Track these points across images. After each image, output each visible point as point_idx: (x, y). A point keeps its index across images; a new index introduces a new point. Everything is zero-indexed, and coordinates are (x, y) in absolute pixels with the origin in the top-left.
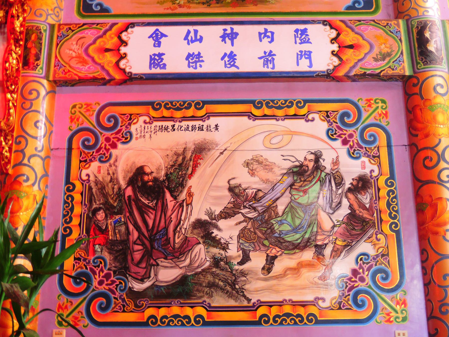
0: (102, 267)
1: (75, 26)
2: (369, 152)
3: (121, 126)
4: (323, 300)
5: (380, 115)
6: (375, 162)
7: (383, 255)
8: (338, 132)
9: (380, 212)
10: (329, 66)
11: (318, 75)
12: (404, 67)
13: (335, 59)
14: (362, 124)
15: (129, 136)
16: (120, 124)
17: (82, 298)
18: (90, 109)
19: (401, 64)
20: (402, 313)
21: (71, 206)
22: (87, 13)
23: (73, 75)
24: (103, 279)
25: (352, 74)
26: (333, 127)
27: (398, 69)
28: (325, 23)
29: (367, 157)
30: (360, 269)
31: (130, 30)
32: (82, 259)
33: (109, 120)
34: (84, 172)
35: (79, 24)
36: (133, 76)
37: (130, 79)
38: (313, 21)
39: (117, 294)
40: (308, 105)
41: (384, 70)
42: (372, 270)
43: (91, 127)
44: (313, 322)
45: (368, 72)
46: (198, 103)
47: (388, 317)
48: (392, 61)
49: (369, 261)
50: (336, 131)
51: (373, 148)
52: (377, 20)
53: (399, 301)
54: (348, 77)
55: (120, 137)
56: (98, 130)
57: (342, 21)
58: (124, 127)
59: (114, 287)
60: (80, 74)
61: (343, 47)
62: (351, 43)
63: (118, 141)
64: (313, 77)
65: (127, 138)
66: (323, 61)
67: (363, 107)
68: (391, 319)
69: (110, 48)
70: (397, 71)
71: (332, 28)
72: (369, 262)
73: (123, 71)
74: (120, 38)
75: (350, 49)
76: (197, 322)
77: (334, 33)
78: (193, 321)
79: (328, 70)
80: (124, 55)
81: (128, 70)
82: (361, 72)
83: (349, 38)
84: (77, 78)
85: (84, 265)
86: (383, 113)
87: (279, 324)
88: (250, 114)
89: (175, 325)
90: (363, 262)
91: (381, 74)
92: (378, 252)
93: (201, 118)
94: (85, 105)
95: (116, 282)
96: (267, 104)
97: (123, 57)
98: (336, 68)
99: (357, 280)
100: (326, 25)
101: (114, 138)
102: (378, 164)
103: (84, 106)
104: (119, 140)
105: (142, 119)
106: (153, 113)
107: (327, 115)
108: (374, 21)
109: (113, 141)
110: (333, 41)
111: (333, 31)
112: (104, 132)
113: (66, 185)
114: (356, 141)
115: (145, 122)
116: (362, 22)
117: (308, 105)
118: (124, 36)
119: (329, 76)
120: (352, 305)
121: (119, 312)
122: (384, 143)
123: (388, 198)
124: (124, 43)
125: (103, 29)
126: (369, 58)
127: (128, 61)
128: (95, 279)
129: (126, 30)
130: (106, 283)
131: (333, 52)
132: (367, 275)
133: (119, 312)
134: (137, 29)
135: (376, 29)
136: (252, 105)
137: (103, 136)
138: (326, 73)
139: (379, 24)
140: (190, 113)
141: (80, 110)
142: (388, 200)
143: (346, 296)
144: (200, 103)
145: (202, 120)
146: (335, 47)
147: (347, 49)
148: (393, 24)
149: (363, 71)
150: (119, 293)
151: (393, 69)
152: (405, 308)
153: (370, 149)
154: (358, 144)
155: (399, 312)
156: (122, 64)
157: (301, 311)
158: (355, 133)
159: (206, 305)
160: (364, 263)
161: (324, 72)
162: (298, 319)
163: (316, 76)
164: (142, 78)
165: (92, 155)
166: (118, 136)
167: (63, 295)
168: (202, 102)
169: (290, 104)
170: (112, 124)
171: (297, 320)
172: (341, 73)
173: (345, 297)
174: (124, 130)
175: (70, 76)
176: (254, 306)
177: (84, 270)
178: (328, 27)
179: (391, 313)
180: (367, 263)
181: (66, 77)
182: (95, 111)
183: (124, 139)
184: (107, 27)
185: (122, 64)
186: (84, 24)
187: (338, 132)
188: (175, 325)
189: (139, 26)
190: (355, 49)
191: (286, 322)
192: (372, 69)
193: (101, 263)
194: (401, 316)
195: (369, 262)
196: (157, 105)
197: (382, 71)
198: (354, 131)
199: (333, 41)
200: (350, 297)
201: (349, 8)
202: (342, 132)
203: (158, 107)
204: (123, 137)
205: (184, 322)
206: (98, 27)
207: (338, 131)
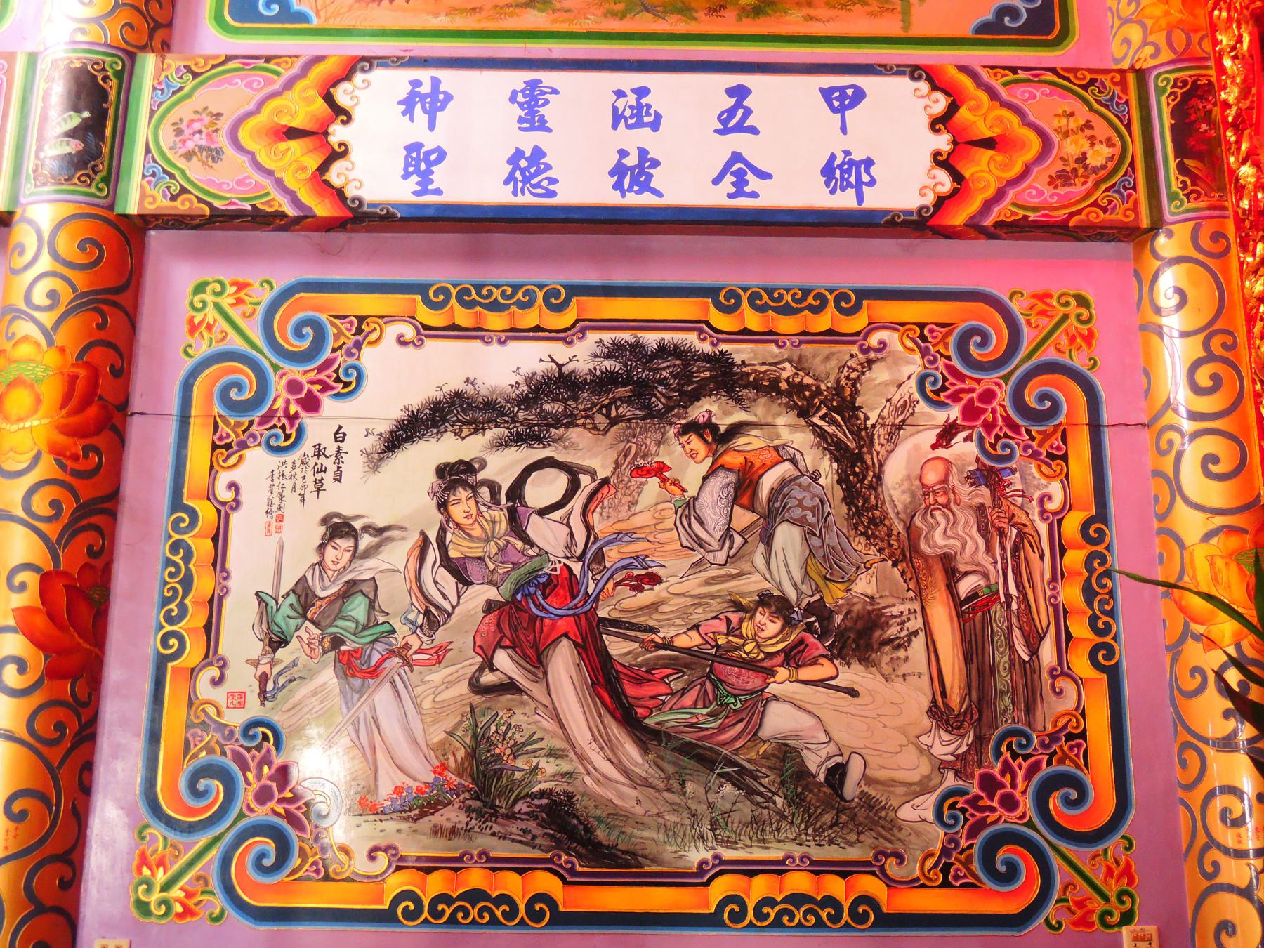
0: (268, 750)
1: (202, 62)
2: (217, 742)
3: (971, 846)
4: (401, 341)
5: (161, 863)
6: (203, 710)
7: (228, 446)
8: (953, 384)
9: (1066, 612)
10: (923, 195)
11: (892, 223)
12: (1136, 202)
13: (943, 177)
14: (1023, 361)
15: (353, 379)
16: (975, 852)
17: (202, 840)
18: (246, 298)
19: (1129, 196)
20: (204, 303)
21: (1096, 604)
22: (240, 21)
23: (195, 200)
24: (269, 783)
25: (988, 222)
26: (937, 369)
27: (1121, 208)
28: (914, 72)
29: (227, 726)
30: (296, 415)
31: (359, 77)
32: (1042, 457)
33: (298, 334)
34: (1069, 702)
35: (217, 57)
36: (365, 209)
37: (358, 220)
38: (884, 66)
39: (941, 367)
40: (382, 903)
41: (1080, 212)
42: (263, 411)
43: (1064, 846)
44: (435, 287)
45: (1032, 216)
46: (737, 917)
47: (242, 295)
48: (1104, 187)
49: (267, 433)
50: (945, 379)
51: (204, 754)
52: (1064, 69)
53: (1114, 866)
54: (975, 229)
55: (330, 382)
56: (267, 358)
57: (963, 69)
58: (964, 844)
59: (298, 808)
60: (218, 204)
61: (965, 143)
62: (989, 134)
63: (978, 797)
64: (878, 225)
65: (350, 383)
66: (905, 182)
67: (211, 893)
68: (234, 289)
69: (301, 127)
70: (1113, 217)
71: (935, 87)
72: (1030, 756)
73: (340, 193)
74: (329, 99)
75: (983, 150)
76: (732, 294)
77: (940, 103)
78: (745, 297)
79: (920, 209)
80: (343, 148)
81: (350, 192)
82: (1014, 213)
83: (980, 118)
84: (208, 212)
85: (217, 742)
86: (150, 869)
87: (521, 286)
88: (569, 879)
89: (788, 290)
90: (284, 430)
91: (1071, 224)
92: (240, 457)
93: (725, 868)
94: (1093, 924)
95: (947, 397)
96: (511, 915)
97: (337, 154)
98: (941, 202)
99: (995, 804)
100: (919, 78)
101: (312, 382)
102: (1063, 476)
103: (1095, 917)
104: (326, 388)
105: (392, 331)
106: (426, 315)
107: (921, 335)
108: (1053, 70)
109: (309, 391)
110: (937, 124)
111: (939, 96)
112: (286, 366)
113: (172, 514)
114: (250, 776)
115: (401, 341)
116: (1022, 75)
117: (382, 903)
118: (342, 95)
119: (921, 226)
120: (328, 324)
121: (937, 324)
122: (1083, 417)
123: (187, 601)
124: (341, 113)
125: (286, 75)
126: (1039, 179)
127: (353, 164)
128: (248, 783)
129: (347, 75)
130: (974, 395)
131: (936, 155)
132: (1024, 792)
133: (937, 324)
134: (379, 75)
135: (1061, 96)
136: (561, 909)
137: (281, 377)
138: (915, 217)
139: (1067, 79)
140: (760, 887)
141: (1107, 907)
142: (185, 595)
143: (340, 348)
144: (559, 292)
145: (723, 862)
146: (943, 142)
147: (975, 148)
148: (1108, 84)
149: (1022, 213)
150: (937, 369)
151: (1105, 210)
152: (193, 313)
153: (210, 751)
154: (245, 768)
155: (210, 306)
156: (335, 175)
157: (463, 317)
158: (248, 806)
159: (560, 866)
160: (1015, 756)
161: (910, 212)
162: (827, 910)
163: (887, 222)
164: (394, 216)
165: (248, 429)
166: (322, 376)
167: (1084, 369)
168: (722, 925)
169: (440, 907)
170: (1002, 855)
171: (824, 915)
172: (959, 217)
173: (961, 853)
174: (964, 833)
175: (187, 204)
176: (583, 331)
177: (1034, 429)
178: (924, 86)
179: (232, 305)
180: (1025, 758)
181: (176, 208)
182: (1057, 902)
183: (341, 385)
184: (295, 70)
185: (335, 175)
186: (228, 59)
187: (953, 384)
188: (788, 290)
189: (385, 66)
190: (999, 151)
191: (791, 920)
192: (1044, 208)
193: (265, 738)
194: (209, 298)
195: (1030, 756)
196: (436, 295)
197: (1072, 215)
198: (251, 810)
199: (937, 124)
200: (330, 344)
201: (983, 28)
202: (287, 806)
203: (442, 297)
204: (338, 380)
205: (499, 914)
206: (271, 66)
207: (952, 380)
